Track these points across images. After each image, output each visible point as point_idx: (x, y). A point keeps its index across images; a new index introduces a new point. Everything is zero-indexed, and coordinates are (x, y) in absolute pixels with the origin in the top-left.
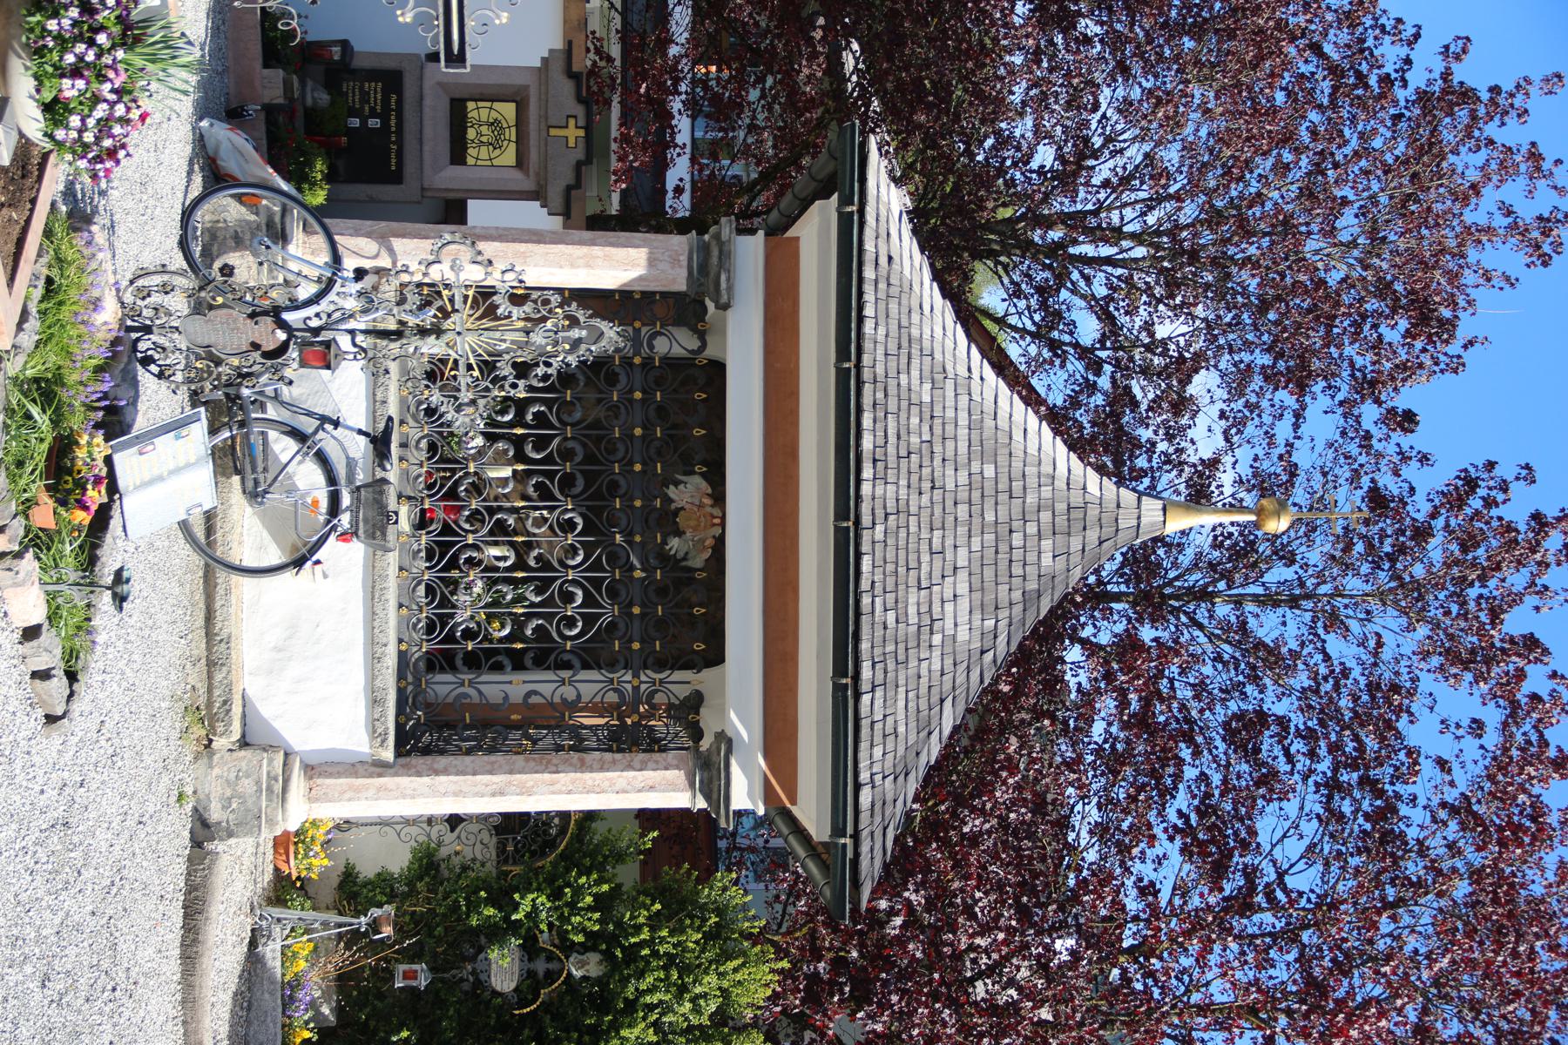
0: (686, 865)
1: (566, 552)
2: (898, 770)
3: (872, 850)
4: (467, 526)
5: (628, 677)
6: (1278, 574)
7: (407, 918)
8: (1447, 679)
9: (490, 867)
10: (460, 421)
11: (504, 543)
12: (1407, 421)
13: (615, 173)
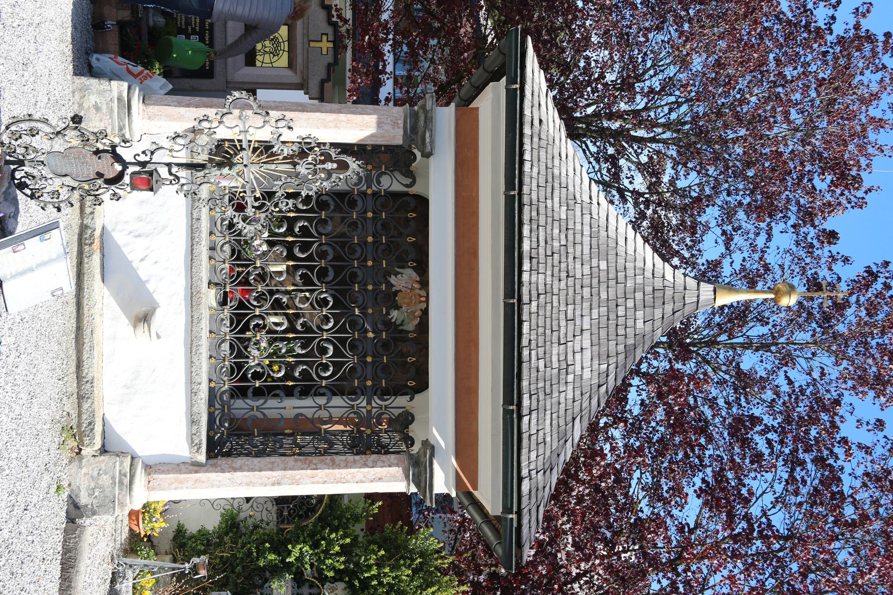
0: (400, 523)
1: (322, 321)
2: (546, 466)
3: (530, 522)
4: (255, 303)
5: (364, 404)
6: (757, 331)
7: (218, 561)
8: (857, 394)
9: (272, 526)
10: (248, 230)
11: (281, 314)
12: (832, 236)
13: (349, 91)
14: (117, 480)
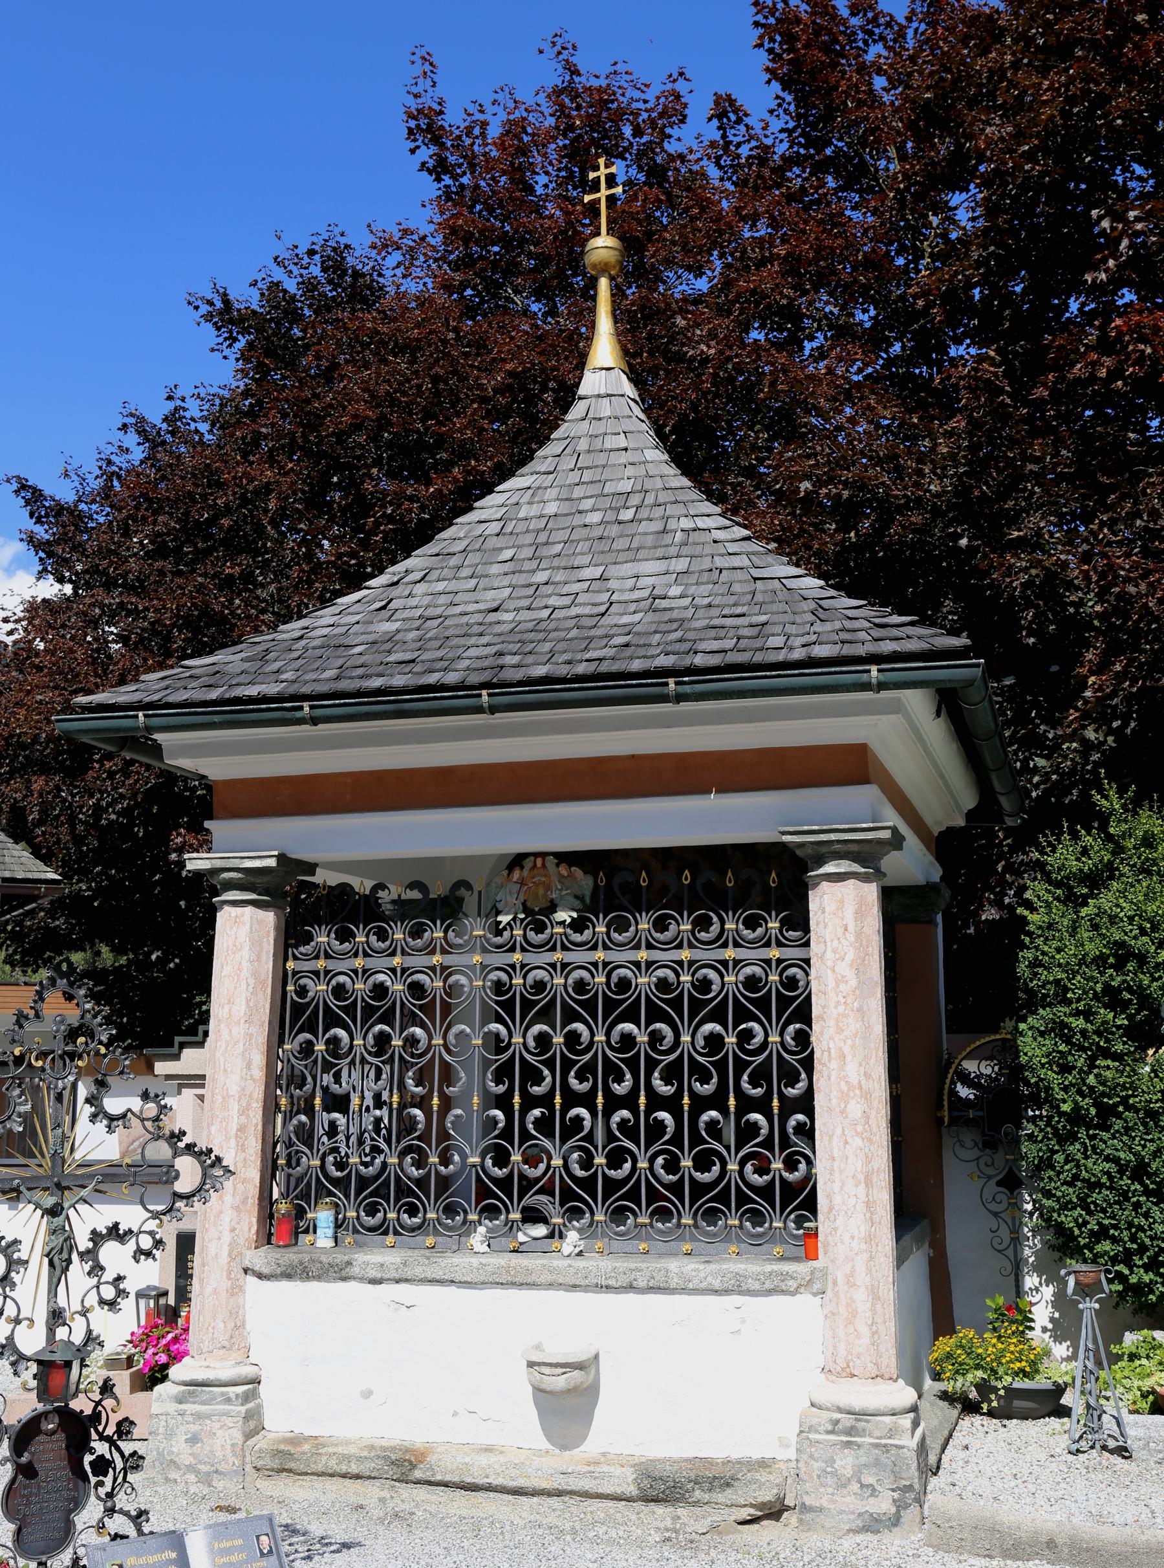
14: (845, 1439)
